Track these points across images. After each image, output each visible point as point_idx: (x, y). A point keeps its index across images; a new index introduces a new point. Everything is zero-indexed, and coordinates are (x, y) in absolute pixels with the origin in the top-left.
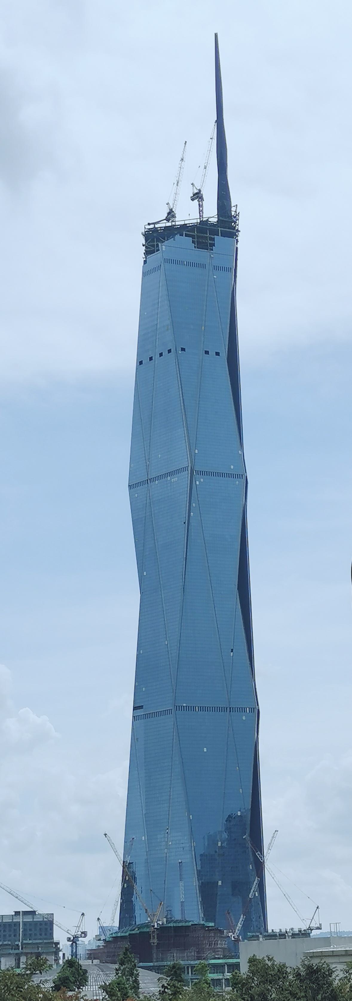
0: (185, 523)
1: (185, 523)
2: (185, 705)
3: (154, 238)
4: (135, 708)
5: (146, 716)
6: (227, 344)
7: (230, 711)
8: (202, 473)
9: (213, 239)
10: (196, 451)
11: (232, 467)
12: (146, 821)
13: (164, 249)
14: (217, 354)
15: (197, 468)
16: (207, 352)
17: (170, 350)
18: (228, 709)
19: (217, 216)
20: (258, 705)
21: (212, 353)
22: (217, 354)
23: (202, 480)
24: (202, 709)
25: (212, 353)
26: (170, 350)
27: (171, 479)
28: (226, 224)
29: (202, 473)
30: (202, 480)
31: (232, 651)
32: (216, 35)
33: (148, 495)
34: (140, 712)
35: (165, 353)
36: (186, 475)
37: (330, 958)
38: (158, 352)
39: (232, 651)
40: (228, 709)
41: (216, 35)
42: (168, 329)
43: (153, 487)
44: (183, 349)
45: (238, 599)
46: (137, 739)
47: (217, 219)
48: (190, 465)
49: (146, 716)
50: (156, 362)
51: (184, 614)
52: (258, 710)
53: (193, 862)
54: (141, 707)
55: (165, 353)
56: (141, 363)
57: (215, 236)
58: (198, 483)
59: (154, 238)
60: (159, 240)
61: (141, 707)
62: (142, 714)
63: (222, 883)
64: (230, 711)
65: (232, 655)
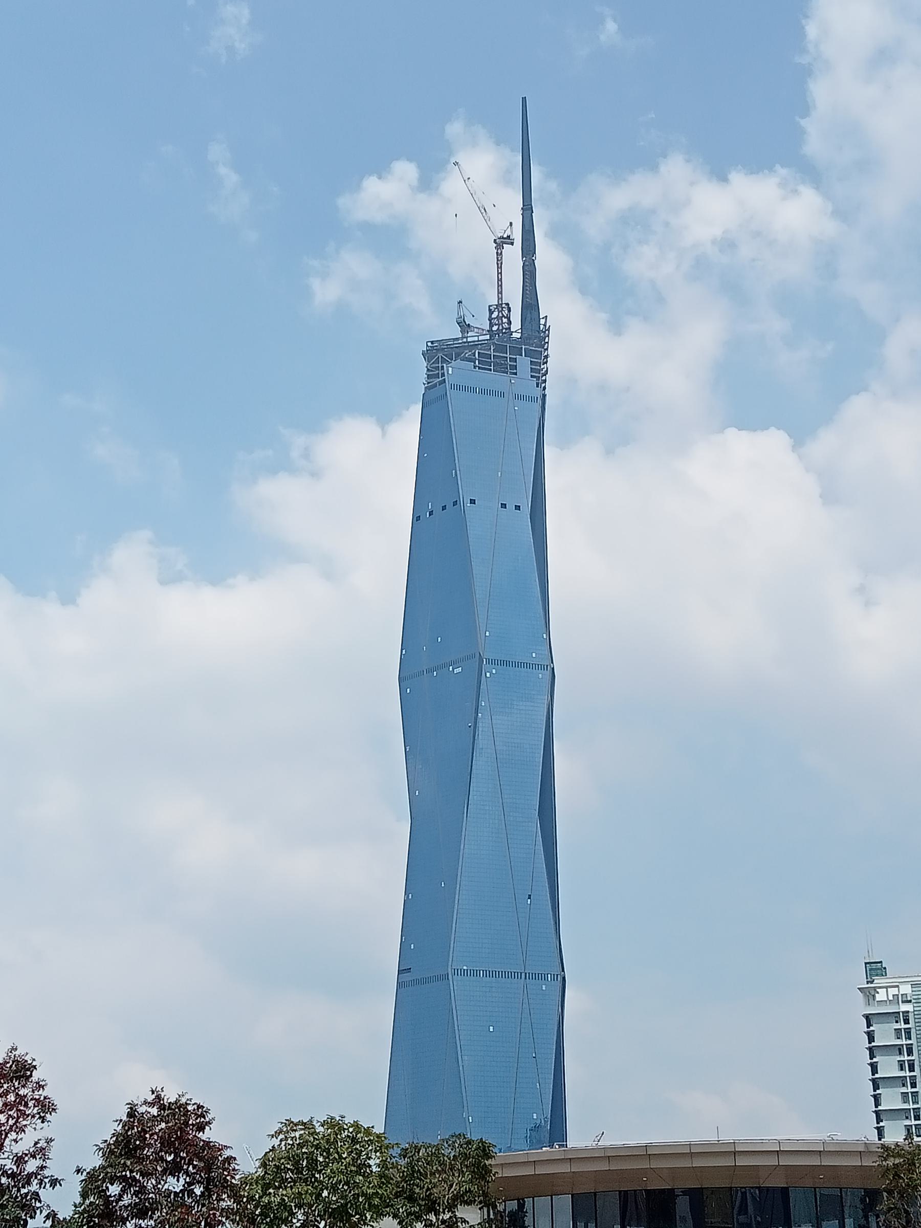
8: (532, 399)
10: (487, 634)
13: (450, 372)
14: (518, 508)
18: (523, 975)
20: (563, 970)
21: (511, 507)
22: (518, 508)
23: (494, 671)
24: (474, 390)
25: (511, 507)
28: (536, 336)
29: (532, 399)
30: (494, 671)
32: (524, 99)
34: (407, 977)
40: (523, 975)
41: (524, 99)
44: (473, 502)
52: (564, 978)
56: (418, 518)
58: (488, 675)
60: (444, 361)
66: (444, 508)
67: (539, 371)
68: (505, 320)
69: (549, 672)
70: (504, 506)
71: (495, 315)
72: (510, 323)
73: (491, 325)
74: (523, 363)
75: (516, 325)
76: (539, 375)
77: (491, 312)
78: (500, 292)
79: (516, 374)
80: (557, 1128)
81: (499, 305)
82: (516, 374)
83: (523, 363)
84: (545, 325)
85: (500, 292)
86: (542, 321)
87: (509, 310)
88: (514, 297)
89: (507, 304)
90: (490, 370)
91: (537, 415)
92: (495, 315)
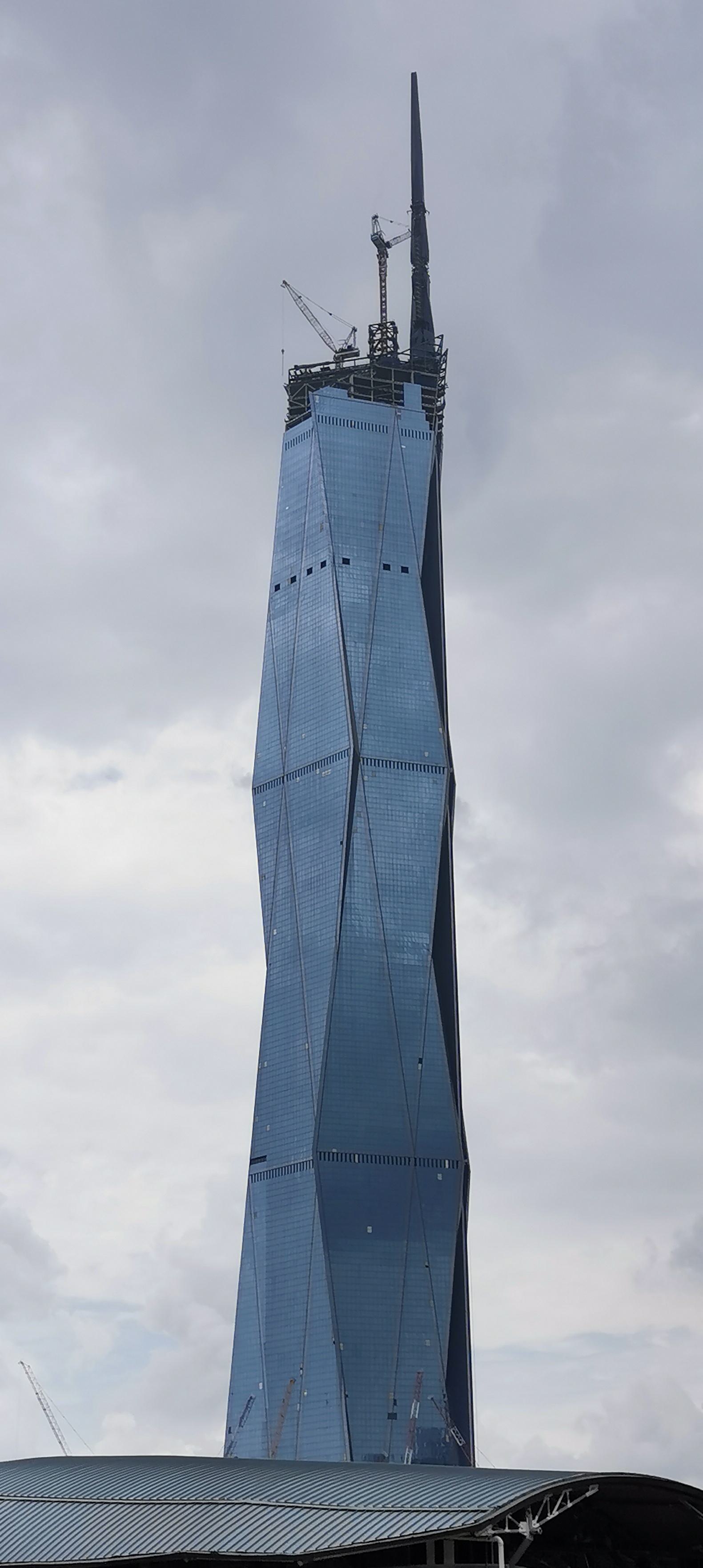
0: (342, 843)
1: (342, 843)
2: (334, 1151)
3: (303, 386)
4: (253, 1161)
5: (271, 1174)
6: (422, 554)
7: (416, 1165)
9: (401, 388)
11: (426, 754)
12: (268, 1375)
14: (405, 570)
15: (365, 753)
16: (387, 567)
17: (325, 562)
18: (412, 1160)
19: (408, 352)
21: (396, 568)
22: (405, 570)
26: (325, 562)
27: (321, 773)
31: (421, 1061)
32: (414, 76)
33: (284, 801)
34: (261, 1167)
35: (317, 568)
36: (346, 763)
37: (407, 269)
38: (305, 566)
39: (421, 1061)
40: (412, 1160)
41: (414, 76)
42: (322, 529)
43: (292, 787)
44: (346, 561)
45: (433, 974)
46: (255, 1214)
47: (409, 357)
48: (352, 746)
49: (271, 1174)
50: (302, 584)
51: (337, 995)
53: (342, 1418)
54: (263, 1158)
55: (317, 568)
56: (277, 588)
57: (405, 383)
59: (303, 386)
61: (263, 1158)
62: (265, 1169)
63: (367, 1230)
64: (416, 1165)
65: (420, 1068)
66: (310, 571)
67: (432, 402)
68: (390, 343)
69: (445, 777)
70: (387, 567)
71: (378, 336)
72: (396, 346)
73: (373, 349)
74: (413, 392)
75: (404, 341)
76: (434, 415)
77: (372, 334)
78: (383, 311)
79: (402, 404)
80: (449, 1440)
81: (382, 326)
82: (402, 404)
83: (413, 392)
84: (440, 346)
85: (383, 311)
86: (437, 341)
87: (395, 331)
88: (401, 313)
89: (393, 323)
90: (370, 399)
91: (430, 455)
92: (378, 336)
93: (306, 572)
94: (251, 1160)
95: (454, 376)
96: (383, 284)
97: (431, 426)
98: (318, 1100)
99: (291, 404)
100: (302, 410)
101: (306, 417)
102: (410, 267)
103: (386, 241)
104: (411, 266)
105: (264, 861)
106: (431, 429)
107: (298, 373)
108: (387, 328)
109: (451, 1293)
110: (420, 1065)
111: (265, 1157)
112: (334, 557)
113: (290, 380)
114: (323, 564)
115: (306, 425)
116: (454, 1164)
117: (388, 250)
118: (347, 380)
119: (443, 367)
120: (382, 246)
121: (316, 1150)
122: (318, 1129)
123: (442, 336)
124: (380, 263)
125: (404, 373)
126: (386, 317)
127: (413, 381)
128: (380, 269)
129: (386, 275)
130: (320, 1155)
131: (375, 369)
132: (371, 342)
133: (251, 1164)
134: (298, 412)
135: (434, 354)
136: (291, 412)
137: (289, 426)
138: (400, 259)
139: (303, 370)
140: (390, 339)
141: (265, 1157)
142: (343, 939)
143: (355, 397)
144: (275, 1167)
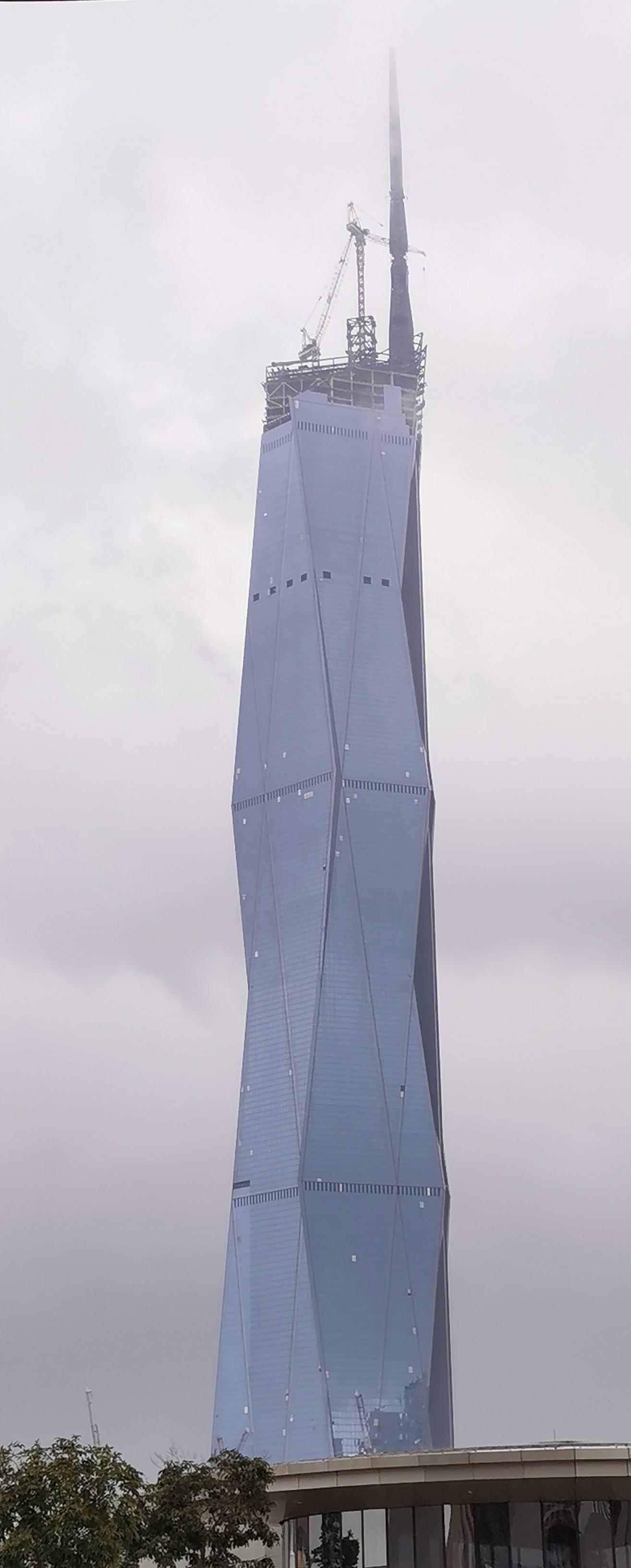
0: (324, 868)
2: (319, 1180)
4: (236, 1186)
5: (254, 1199)
7: (398, 1193)
9: (381, 390)
14: (385, 583)
15: (347, 774)
19: (388, 352)
21: (376, 581)
22: (385, 583)
34: (244, 1192)
35: (297, 581)
36: (327, 788)
40: (395, 1188)
44: (327, 575)
46: (239, 1239)
49: (254, 1199)
53: (321, 661)
54: (246, 1183)
55: (297, 581)
56: (256, 597)
57: (385, 386)
61: (246, 1183)
64: (398, 1193)
66: (290, 583)
68: (368, 338)
70: (367, 580)
75: (383, 345)
79: (383, 408)
81: (360, 319)
84: (420, 345)
86: (417, 340)
87: (374, 325)
88: (380, 309)
89: (371, 318)
90: (350, 403)
92: (355, 331)
93: (286, 584)
94: (234, 1184)
95: (432, 370)
96: (361, 290)
97: (411, 431)
98: (303, 1134)
99: (268, 403)
100: (278, 412)
101: (285, 420)
102: (390, 257)
103: (362, 228)
104: (391, 255)
105: (246, 1112)
106: (411, 434)
107: (276, 370)
108: (365, 322)
109: (433, 1320)
110: (402, 1093)
111: (249, 1181)
112: (328, 1391)
113: (267, 378)
114: (304, 577)
115: (286, 428)
116: (436, 1191)
117: (365, 237)
118: (328, 383)
119: (422, 364)
120: (359, 234)
121: (301, 1180)
122: (303, 1154)
123: (422, 334)
124: (358, 251)
125: (383, 373)
126: (363, 310)
127: (392, 382)
128: (358, 258)
129: (363, 264)
130: (306, 1185)
131: (354, 370)
132: (349, 336)
133: (234, 1188)
134: (276, 414)
135: (413, 352)
136: (269, 412)
137: (267, 428)
138: (379, 258)
139: (281, 368)
140: (369, 335)
141: (249, 1181)
142: (326, 966)
143: (335, 401)
144: (258, 1193)
